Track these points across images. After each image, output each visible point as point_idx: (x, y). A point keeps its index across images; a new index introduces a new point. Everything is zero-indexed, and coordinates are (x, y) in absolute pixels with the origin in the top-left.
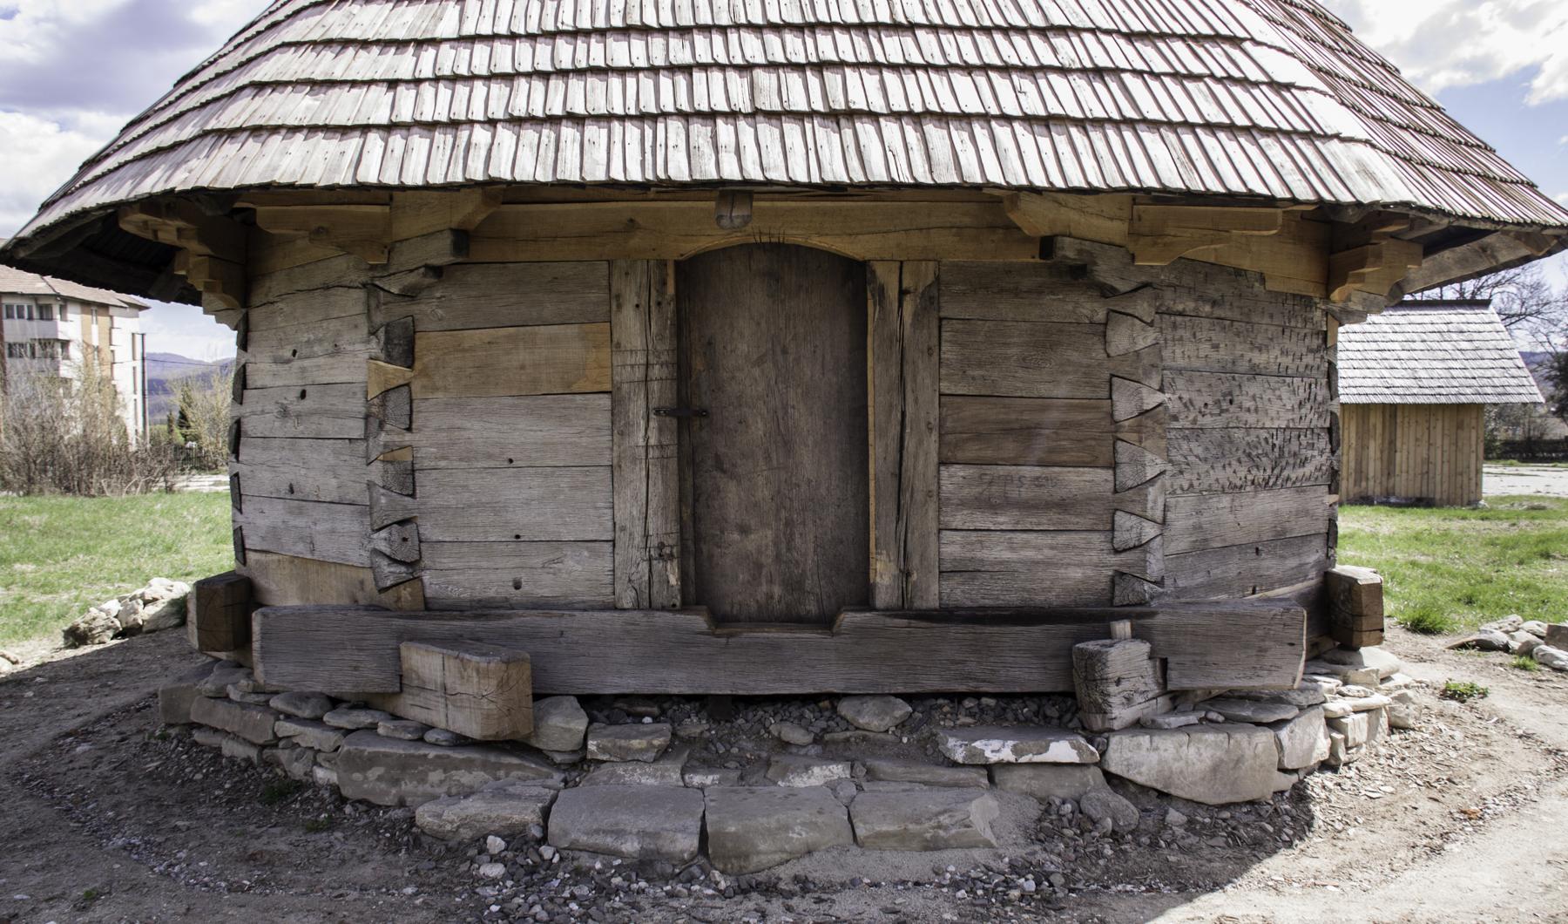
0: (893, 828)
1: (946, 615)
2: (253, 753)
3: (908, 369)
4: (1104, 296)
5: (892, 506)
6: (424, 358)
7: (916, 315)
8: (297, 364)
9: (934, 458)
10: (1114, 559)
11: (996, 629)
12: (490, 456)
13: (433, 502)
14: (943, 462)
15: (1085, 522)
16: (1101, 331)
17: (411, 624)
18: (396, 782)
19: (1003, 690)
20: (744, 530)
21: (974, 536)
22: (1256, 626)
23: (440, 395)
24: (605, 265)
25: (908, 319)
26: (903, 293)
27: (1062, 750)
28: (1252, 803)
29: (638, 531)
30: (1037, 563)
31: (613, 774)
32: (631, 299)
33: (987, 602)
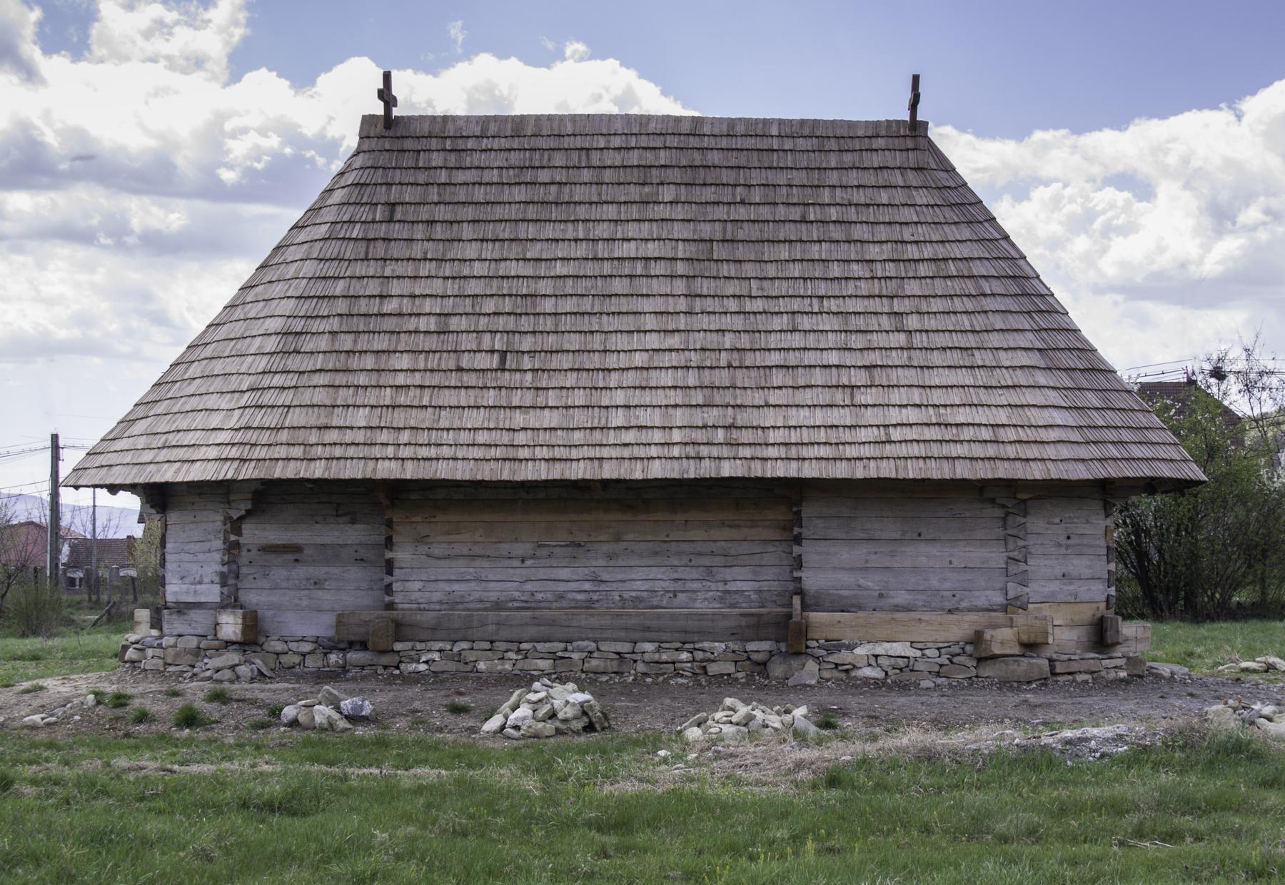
8: (1063, 525)
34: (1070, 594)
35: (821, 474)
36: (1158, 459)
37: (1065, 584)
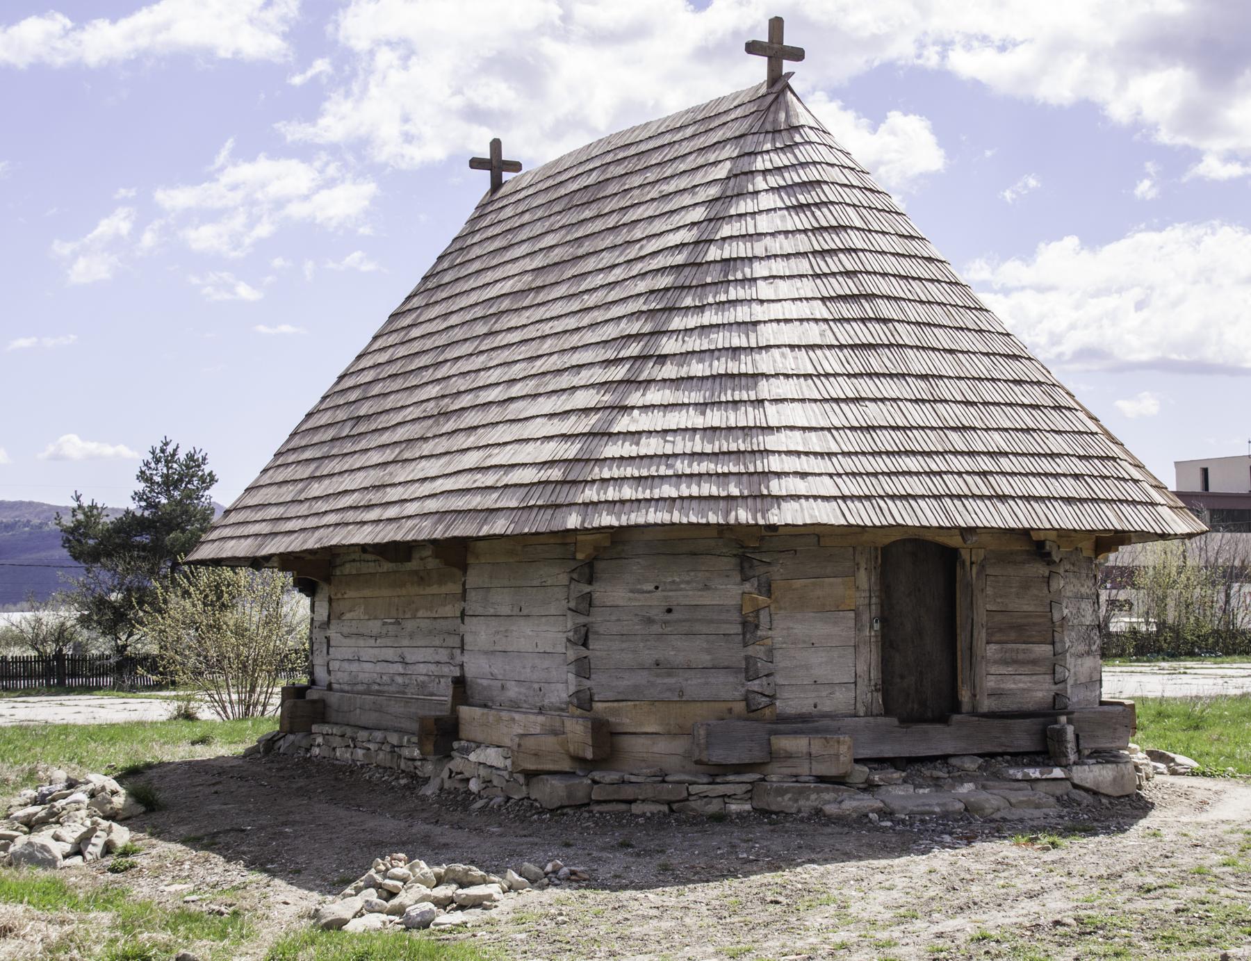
0: (1025, 799)
1: (992, 715)
2: (665, 808)
3: (974, 598)
4: (1048, 564)
5: (968, 663)
6: (776, 594)
7: (978, 574)
8: (659, 593)
9: (984, 641)
10: (1055, 687)
11: (1012, 721)
12: (804, 642)
13: (782, 665)
14: (988, 643)
15: (1042, 670)
16: (1048, 581)
17: (774, 726)
18: (796, 801)
19: (1016, 750)
20: (902, 677)
21: (999, 677)
22: (1112, 718)
23: (782, 611)
24: (851, 549)
25: (974, 576)
26: (972, 563)
27: (1058, 773)
28: (1127, 796)
29: (866, 677)
30: (1024, 690)
31: (888, 791)
32: (863, 565)
33: (1005, 709)
34: (669, 690)
35: (1144, 548)
36: (1127, 501)
37: (657, 676)
